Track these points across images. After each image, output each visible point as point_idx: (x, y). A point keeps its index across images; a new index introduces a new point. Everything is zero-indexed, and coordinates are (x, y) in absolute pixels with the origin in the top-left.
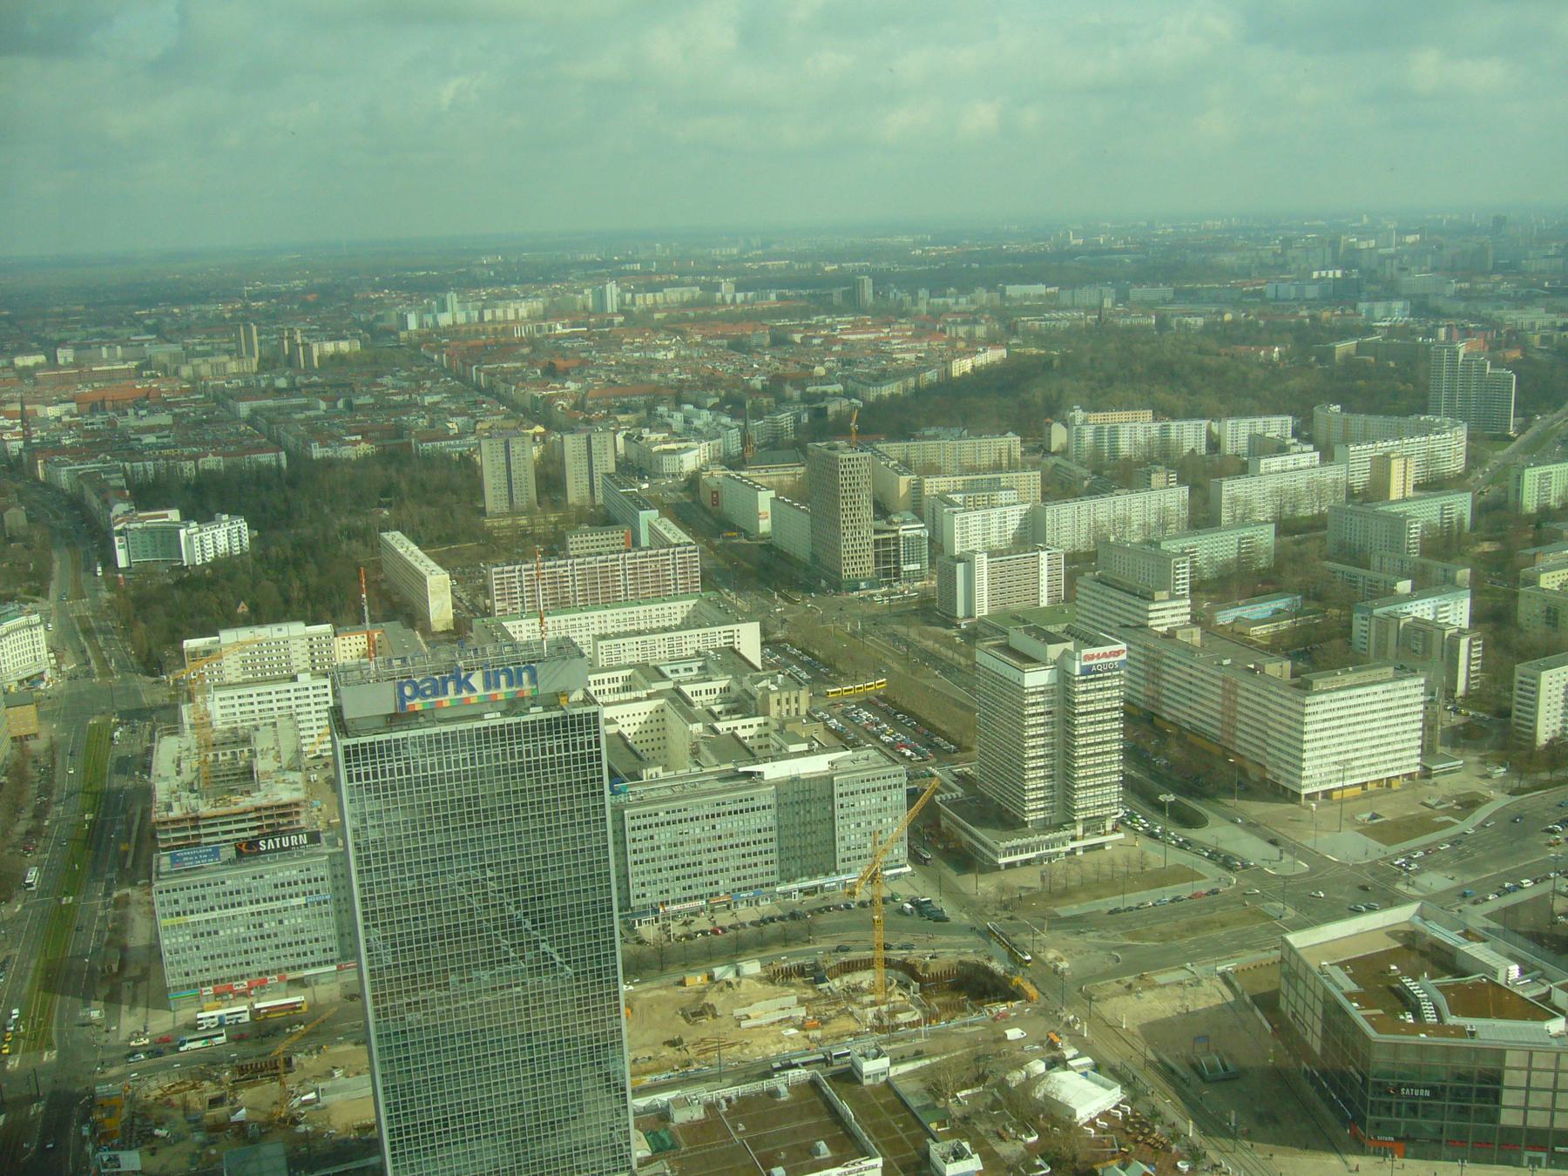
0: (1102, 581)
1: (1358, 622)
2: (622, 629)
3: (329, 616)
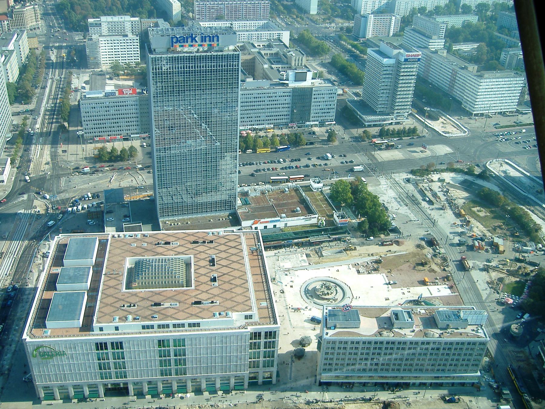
0: (414, 30)
1: (503, 56)
2: (241, 29)
3: (138, 15)
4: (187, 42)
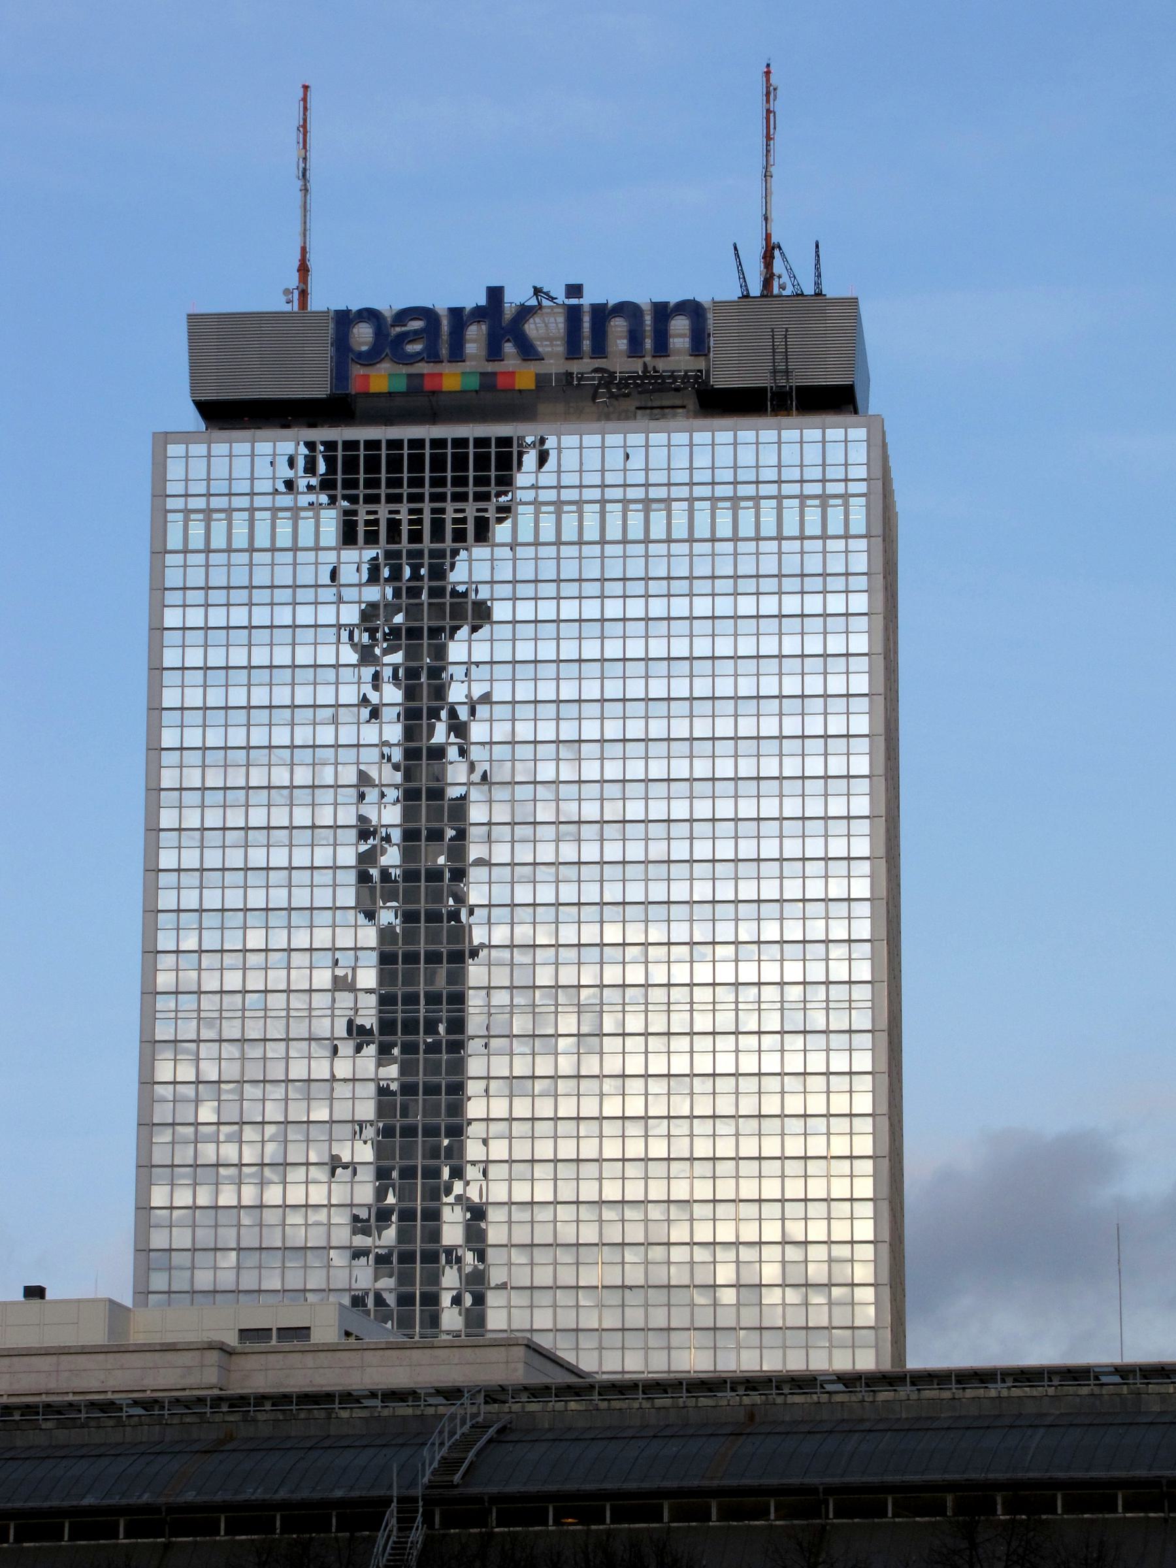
4: (457, 354)
